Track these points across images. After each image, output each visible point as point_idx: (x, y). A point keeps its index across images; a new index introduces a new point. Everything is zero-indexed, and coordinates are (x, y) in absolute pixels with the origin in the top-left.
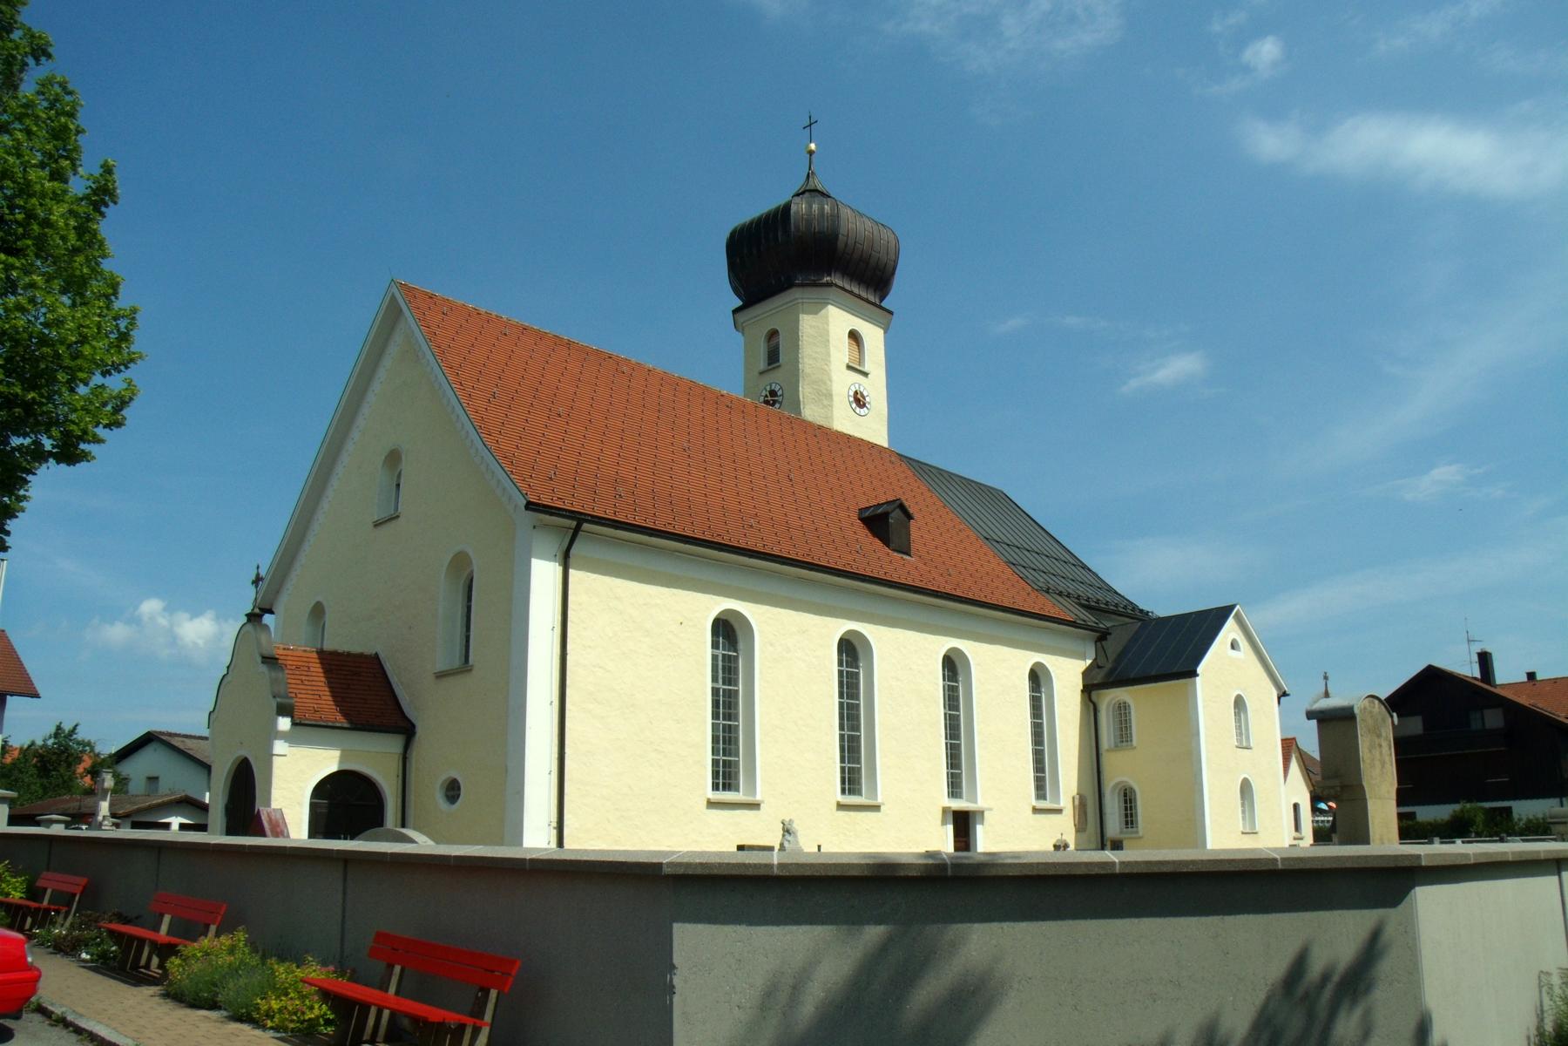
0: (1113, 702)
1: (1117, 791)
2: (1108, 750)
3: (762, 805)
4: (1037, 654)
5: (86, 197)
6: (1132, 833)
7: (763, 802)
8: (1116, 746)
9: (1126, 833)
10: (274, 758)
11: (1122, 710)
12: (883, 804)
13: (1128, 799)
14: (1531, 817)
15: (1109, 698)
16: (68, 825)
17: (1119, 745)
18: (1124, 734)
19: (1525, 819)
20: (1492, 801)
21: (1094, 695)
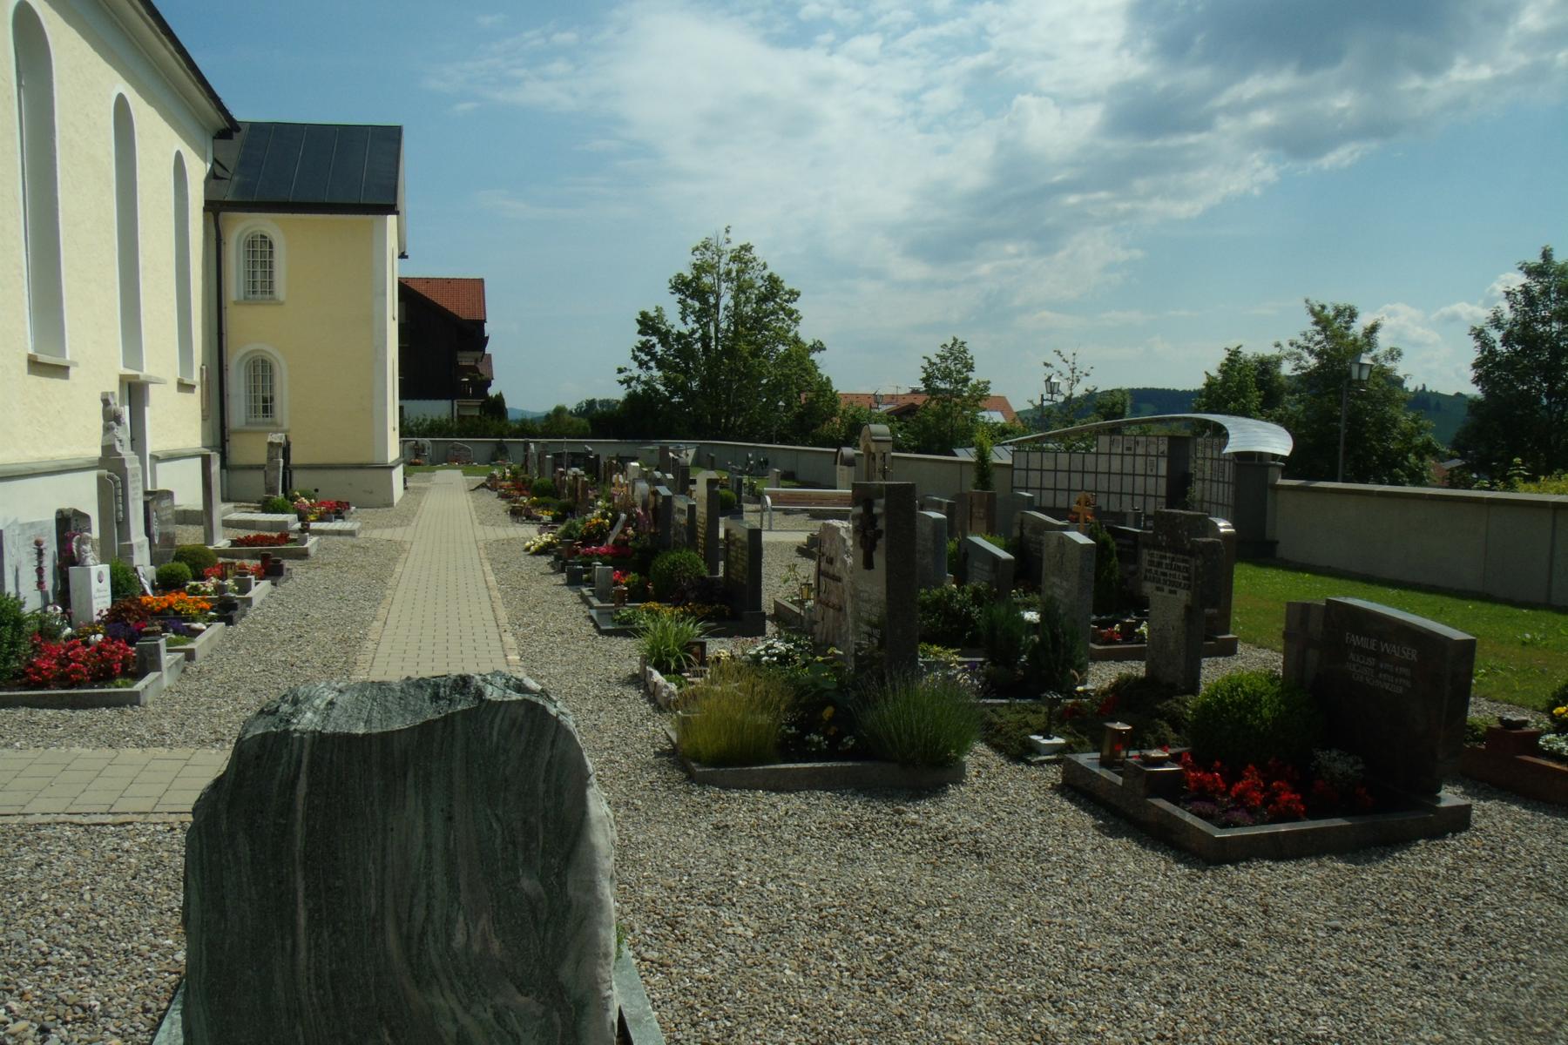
0: (246, 234)
1: (244, 364)
2: (236, 303)
3: (72, 371)
4: (184, 143)
5: (1260, 712)
6: (267, 424)
7: (76, 364)
8: (245, 298)
9: (256, 424)
10: (449, 402)
11: (261, 250)
12: (76, 364)
13: (261, 370)
14: (436, 418)
15: (242, 225)
16: (234, 563)
17: (251, 296)
18: (261, 282)
19: (429, 418)
20: (982, 548)
21: (223, 215)
